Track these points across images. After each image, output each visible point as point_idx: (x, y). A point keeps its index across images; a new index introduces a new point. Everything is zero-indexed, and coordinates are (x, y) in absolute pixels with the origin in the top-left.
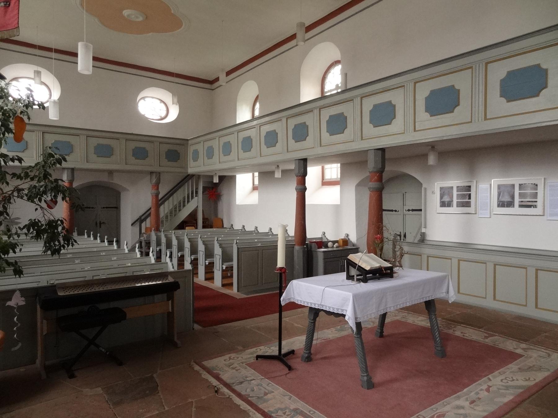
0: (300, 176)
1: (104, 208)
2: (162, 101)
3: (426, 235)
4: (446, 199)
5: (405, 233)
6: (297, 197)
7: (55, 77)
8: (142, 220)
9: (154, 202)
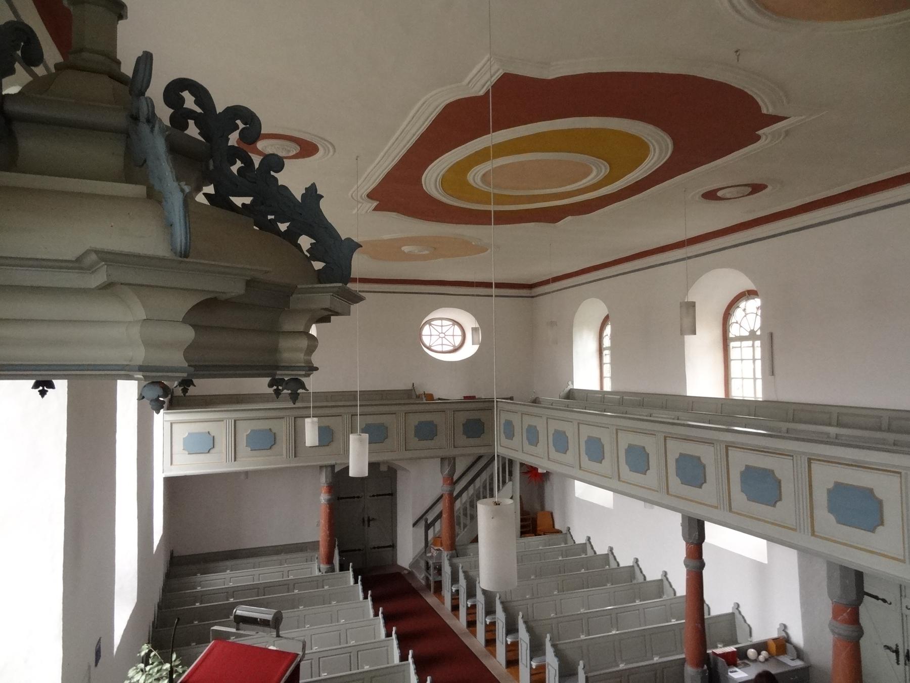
1: (374, 496)
2: (455, 323)
9: (447, 505)
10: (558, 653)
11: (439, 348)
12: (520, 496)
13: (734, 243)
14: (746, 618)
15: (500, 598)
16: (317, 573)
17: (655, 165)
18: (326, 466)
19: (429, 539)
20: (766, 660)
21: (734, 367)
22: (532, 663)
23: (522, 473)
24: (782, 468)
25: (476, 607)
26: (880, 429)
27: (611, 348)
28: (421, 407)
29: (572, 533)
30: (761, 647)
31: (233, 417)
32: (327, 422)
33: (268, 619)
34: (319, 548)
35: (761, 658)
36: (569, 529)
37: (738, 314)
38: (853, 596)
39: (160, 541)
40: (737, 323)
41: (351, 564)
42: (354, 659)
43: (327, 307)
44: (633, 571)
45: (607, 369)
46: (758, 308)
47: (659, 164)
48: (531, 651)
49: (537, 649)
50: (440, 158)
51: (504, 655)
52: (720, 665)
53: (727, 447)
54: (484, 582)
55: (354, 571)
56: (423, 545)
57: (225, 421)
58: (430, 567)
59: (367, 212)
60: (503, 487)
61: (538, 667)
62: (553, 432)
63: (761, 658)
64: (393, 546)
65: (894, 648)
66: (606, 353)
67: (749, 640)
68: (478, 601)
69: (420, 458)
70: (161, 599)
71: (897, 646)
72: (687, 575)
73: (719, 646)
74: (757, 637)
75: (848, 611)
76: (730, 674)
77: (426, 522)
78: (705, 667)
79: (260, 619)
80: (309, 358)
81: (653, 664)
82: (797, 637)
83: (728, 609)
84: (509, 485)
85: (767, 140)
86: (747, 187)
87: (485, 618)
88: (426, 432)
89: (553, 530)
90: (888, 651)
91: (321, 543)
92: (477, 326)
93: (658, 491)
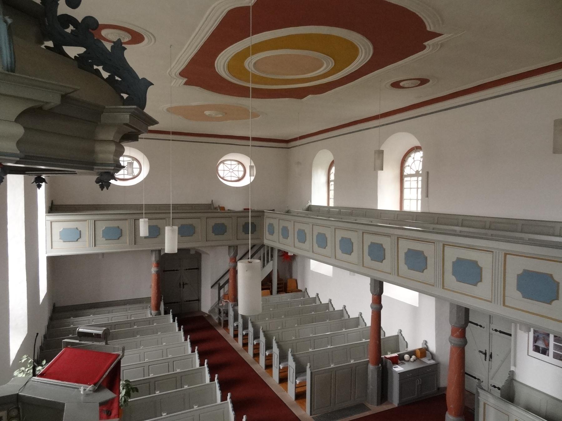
0: (375, 295)
1: (186, 270)
2: (240, 163)
3: (515, 373)
4: (541, 344)
5: (491, 353)
6: (372, 315)
7: (145, 156)
8: (221, 287)
10: (295, 360)
11: (229, 179)
12: (278, 270)
13: (408, 117)
14: (405, 338)
15: (262, 329)
16: (150, 316)
17: (363, 61)
18: (155, 251)
19: (221, 296)
20: (415, 361)
21: (406, 192)
22: (280, 366)
23: (279, 256)
24: (428, 250)
25: (259, 345)
26: (484, 228)
27: (335, 181)
28: (217, 215)
29: (308, 292)
30: (411, 353)
31: (93, 218)
32: (155, 223)
33: (100, 333)
34: (150, 302)
35: (412, 359)
36: (306, 289)
37: (410, 161)
38: (463, 323)
39: (45, 297)
40: (409, 166)
41: (171, 310)
42: (171, 365)
43: (127, 123)
44: (343, 312)
45: (332, 193)
46: (421, 157)
47: (365, 61)
48: (296, 373)
49: (283, 358)
50: (225, 50)
51: (264, 362)
52: (388, 364)
53: (398, 238)
54: (241, 310)
55: (173, 315)
56: (217, 299)
57: (88, 221)
58: (221, 312)
59: (179, 86)
60: (267, 264)
61: (284, 368)
62: (297, 230)
63: (412, 359)
64: (199, 300)
65: (484, 352)
66: (332, 183)
67: (406, 349)
68: (261, 341)
69: (214, 246)
70: (46, 333)
71: (486, 350)
72: (372, 313)
73: (389, 353)
74: (411, 348)
75: (460, 330)
76: (393, 368)
77: (219, 285)
78: (380, 365)
79: (95, 334)
80: (117, 158)
81: (350, 364)
82: (432, 348)
83: (395, 333)
84: (271, 263)
85: (431, 48)
86: (418, 81)
87: (254, 341)
88: (220, 230)
89: (298, 291)
90: (481, 353)
91: (152, 298)
92: (253, 164)
93: (357, 265)
